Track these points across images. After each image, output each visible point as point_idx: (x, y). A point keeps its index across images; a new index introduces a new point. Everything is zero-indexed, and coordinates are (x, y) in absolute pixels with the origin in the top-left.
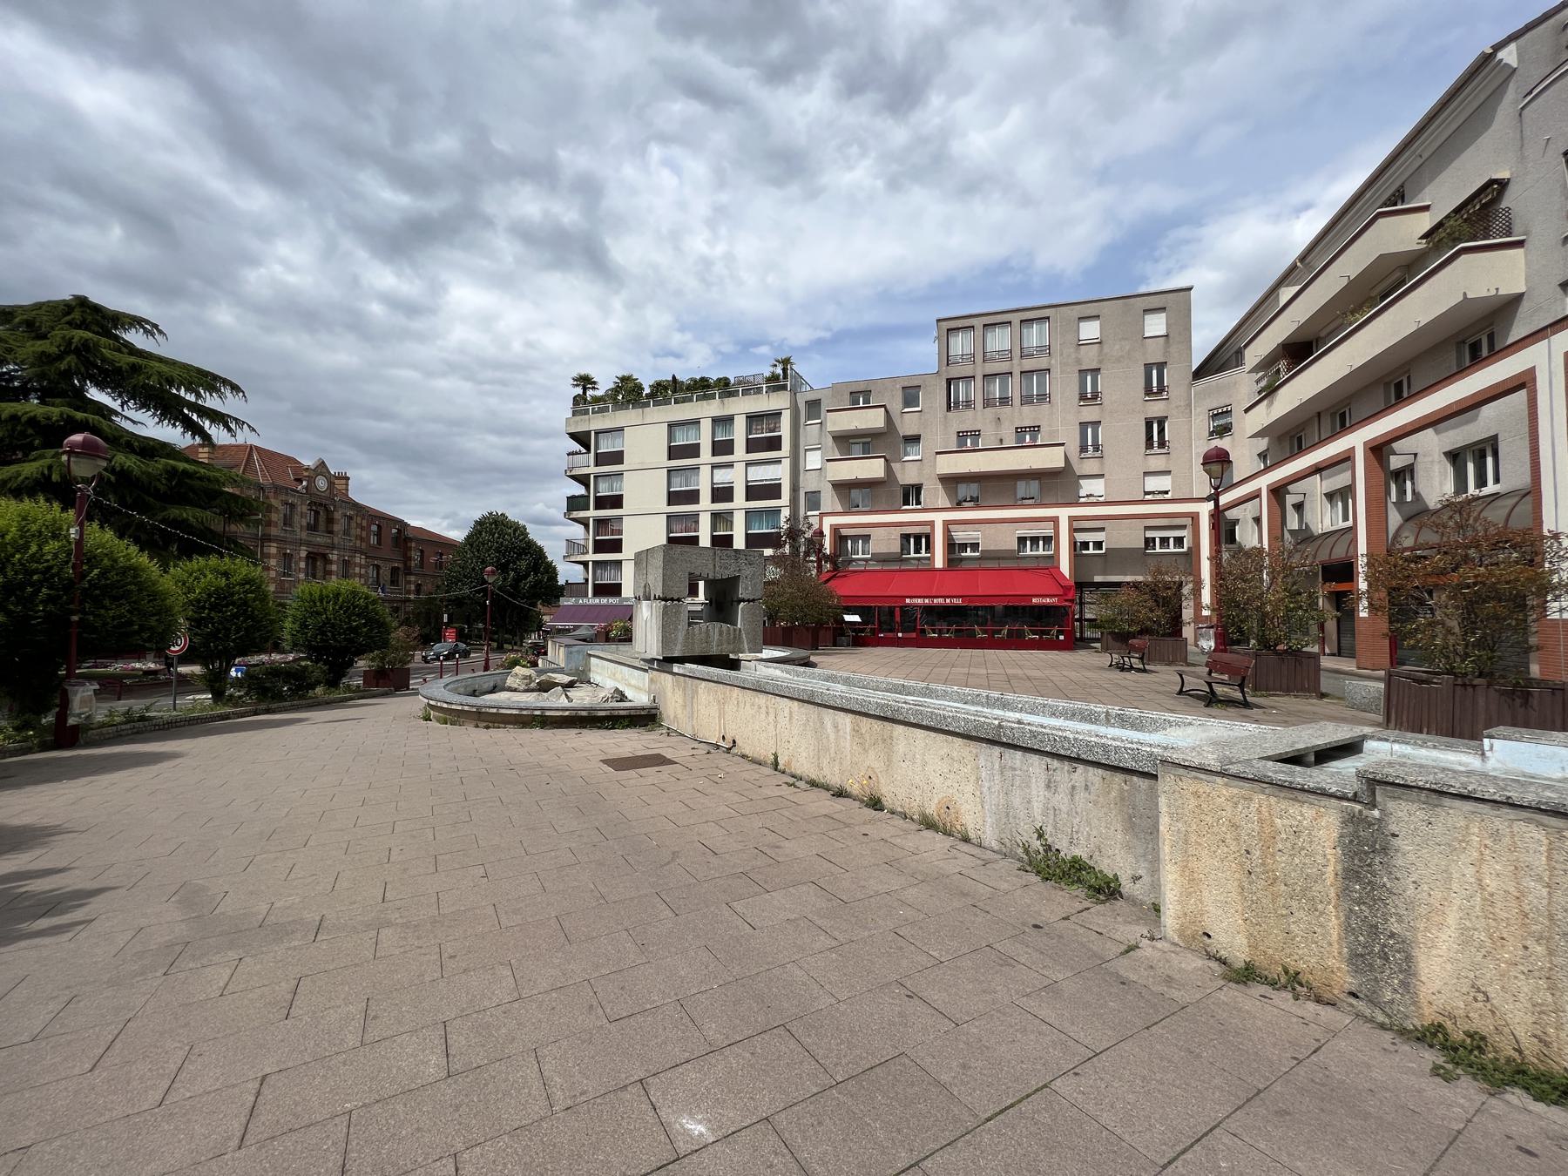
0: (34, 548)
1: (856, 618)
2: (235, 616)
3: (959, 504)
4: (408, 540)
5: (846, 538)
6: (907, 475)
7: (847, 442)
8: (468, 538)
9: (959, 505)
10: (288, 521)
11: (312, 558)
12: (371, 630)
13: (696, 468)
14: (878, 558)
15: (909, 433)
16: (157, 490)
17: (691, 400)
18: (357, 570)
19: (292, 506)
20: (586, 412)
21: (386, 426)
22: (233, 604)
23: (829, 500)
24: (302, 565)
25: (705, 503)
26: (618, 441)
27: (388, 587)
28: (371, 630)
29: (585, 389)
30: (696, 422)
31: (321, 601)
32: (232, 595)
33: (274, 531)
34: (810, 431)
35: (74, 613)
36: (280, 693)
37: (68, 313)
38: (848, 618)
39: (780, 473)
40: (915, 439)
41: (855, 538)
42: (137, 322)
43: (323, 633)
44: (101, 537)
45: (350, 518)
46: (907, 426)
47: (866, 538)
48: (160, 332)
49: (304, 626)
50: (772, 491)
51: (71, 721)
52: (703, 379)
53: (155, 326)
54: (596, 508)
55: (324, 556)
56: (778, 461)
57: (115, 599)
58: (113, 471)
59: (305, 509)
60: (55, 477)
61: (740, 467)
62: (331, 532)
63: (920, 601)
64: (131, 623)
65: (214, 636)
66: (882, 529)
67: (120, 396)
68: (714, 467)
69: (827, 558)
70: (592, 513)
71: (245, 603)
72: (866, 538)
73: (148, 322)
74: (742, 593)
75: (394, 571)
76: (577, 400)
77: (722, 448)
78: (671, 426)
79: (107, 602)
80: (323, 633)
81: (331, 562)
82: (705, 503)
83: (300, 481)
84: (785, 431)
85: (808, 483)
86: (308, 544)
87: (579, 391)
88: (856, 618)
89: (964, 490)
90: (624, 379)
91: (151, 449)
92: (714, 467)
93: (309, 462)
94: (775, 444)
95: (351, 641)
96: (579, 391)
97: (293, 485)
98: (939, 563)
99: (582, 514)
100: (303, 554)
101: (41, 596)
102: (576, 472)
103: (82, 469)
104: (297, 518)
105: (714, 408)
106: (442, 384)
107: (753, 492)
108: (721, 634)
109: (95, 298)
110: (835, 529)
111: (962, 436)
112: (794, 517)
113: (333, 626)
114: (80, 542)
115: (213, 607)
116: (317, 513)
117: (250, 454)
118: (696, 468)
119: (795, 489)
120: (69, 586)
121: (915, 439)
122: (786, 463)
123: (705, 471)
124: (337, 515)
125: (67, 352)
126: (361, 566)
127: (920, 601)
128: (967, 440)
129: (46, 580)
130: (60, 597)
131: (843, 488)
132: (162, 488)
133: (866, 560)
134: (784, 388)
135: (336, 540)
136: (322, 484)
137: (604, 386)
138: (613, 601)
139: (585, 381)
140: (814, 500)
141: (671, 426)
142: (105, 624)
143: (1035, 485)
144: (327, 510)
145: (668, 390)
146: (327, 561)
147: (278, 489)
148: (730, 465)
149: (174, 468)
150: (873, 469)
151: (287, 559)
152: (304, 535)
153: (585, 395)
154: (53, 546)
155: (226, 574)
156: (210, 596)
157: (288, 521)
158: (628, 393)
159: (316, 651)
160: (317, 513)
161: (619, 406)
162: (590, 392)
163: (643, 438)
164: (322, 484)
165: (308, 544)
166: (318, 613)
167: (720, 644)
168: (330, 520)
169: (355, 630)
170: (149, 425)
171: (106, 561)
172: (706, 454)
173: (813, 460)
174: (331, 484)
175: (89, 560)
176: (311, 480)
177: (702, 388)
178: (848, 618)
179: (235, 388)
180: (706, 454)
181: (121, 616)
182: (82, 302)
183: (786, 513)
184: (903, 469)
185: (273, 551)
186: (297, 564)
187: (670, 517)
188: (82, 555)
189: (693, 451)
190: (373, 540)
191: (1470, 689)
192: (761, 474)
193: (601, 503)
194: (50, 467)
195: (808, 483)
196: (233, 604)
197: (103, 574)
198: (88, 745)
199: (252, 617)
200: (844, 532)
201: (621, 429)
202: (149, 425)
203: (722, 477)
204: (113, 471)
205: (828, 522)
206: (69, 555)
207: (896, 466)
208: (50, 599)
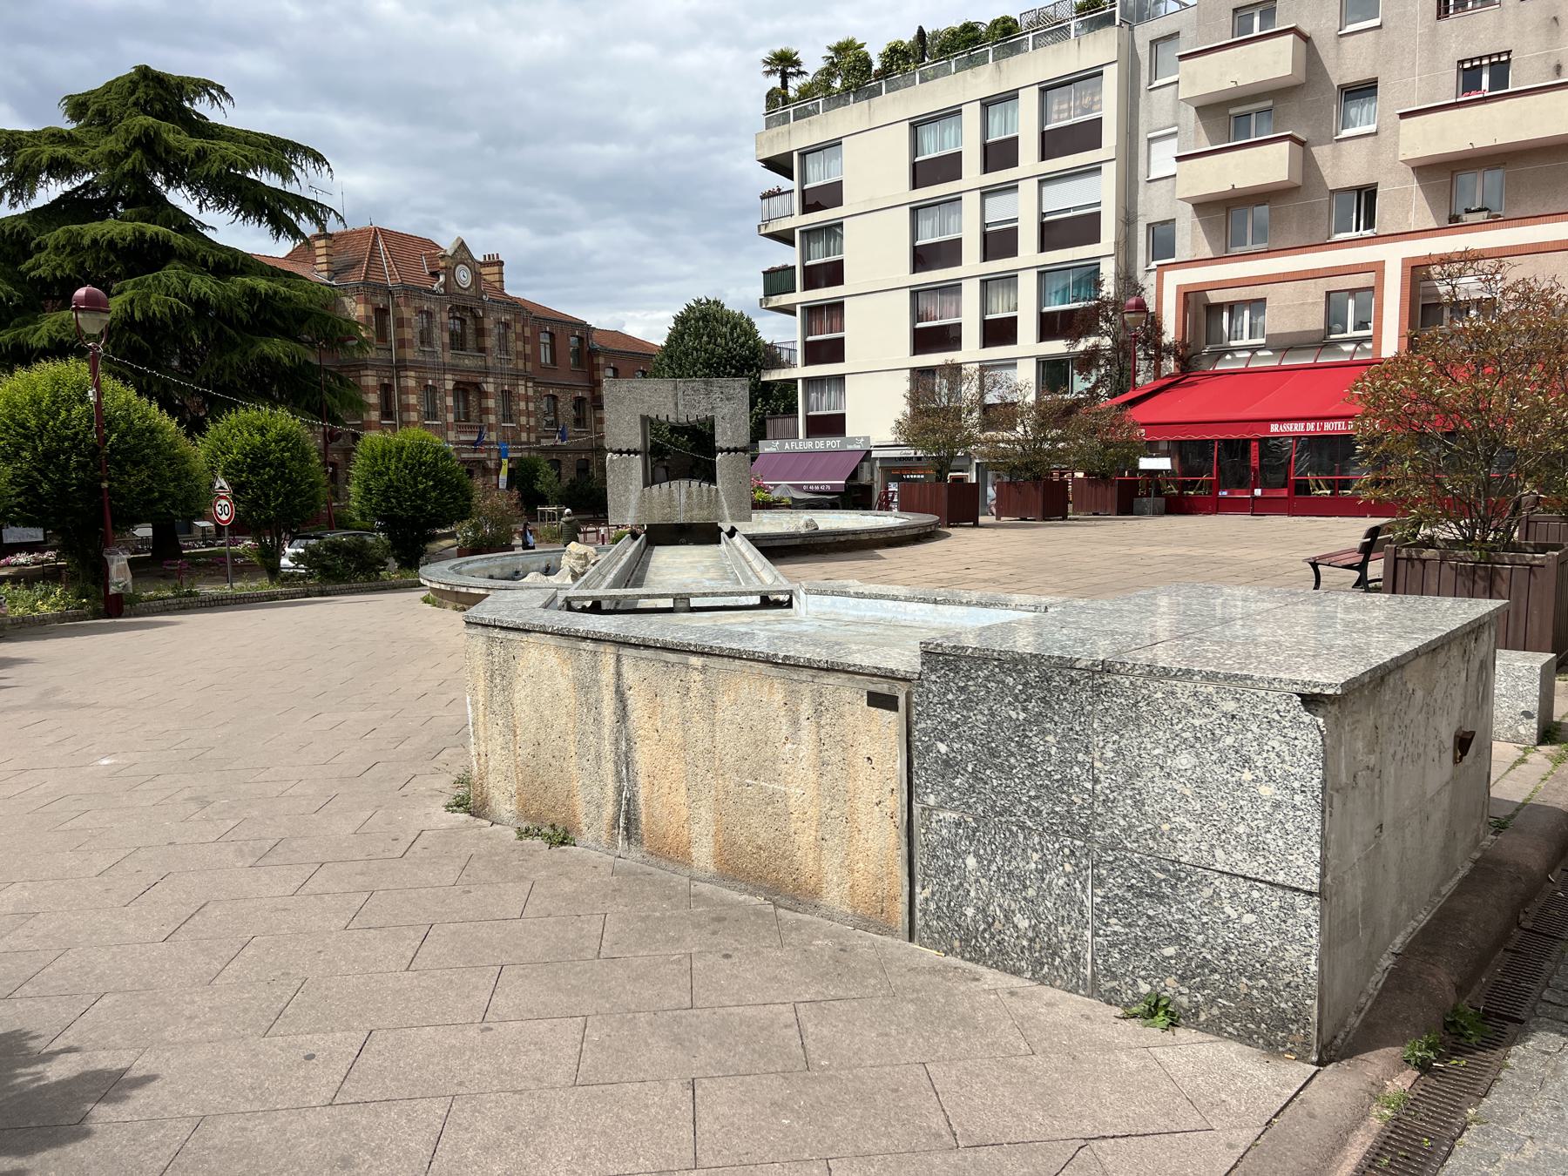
0: (64, 413)
1: (1164, 464)
2: (273, 479)
3: (1454, 219)
4: (593, 353)
5: (1219, 307)
6: (1344, 166)
7: (1229, 117)
8: (669, 340)
9: (1454, 222)
10: (425, 338)
11: (462, 389)
12: (442, 495)
13: (955, 200)
14: (1285, 345)
15: (1350, 79)
16: (240, 320)
17: (947, 72)
18: (522, 405)
19: (429, 314)
20: (786, 120)
21: (613, 152)
22: (271, 465)
23: (1190, 238)
24: (450, 401)
25: (972, 262)
26: (834, 164)
27: (572, 430)
28: (442, 495)
29: (785, 77)
30: (955, 112)
31: (383, 457)
32: (269, 453)
33: (410, 354)
34: (1158, 109)
35: (102, 480)
36: (344, 571)
37: (132, 93)
38: (1146, 464)
39: (1101, 193)
40: (1365, 90)
41: (1233, 307)
42: (203, 87)
43: (387, 500)
44: (121, 395)
45: (507, 325)
46: (1346, 66)
47: (1258, 305)
48: (227, 96)
49: (368, 490)
50: (1084, 228)
51: (113, 590)
52: (969, 28)
53: (221, 89)
54: (806, 287)
55: (477, 386)
56: (1094, 169)
57: (136, 464)
58: (189, 301)
59: (445, 316)
60: (138, 315)
61: (1028, 189)
62: (482, 350)
63: (1298, 427)
64: (150, 490)
65: (254, 503)
66: (1284, 286)
67: (197, 193)
68: (986, 193)
69: (1169, 350)
70: (800, 297)
71: (283, 464)
72: (1258, 305)
73: (213, 85)
74: (720, 442)
75: (579, 402)
76: (775, 99)
77: (999, 154)
78: (915, 125)
79: (128, 468)
80: (387, 500)
81: (485, 395)
82: (972, 262)
83: (435, 275)
84: (1108, 109)
85: (1153, 207)
86: (454, 369)
87: (776, 81)
88: (1164, 464)
89: (1479, 187)
90: (842, 49)
91: (233, 264)
92: (986, 193)
93: (447, 244)
94: (1088, 136)
95: (419, 509)
96: (776, 81)
97: (426, 282)
98: (1390, 345)
99: (785, 300)
100: (450, 385)
101: (73, 464)
102: (770, 229)
103: (92, 324)
104: (436, 332)
105: (982, 80)
106: (691, 60)
107: (1053, 233)
108: (689, 495)
109: (156, 67)
110: (1191, 298)
111: (1469, 75)
112: (1127, 279)
113: (398, 490)
114: (98, 404)
115: (252, 469)
116: (463, 321)
117: (375, 243)
118: (955, 200)
119: (1128, 219)
120: (95, 451)
121: (1365, 90)
122: (1110, 172)
123: (971, 202)
124: (489, 323)
125: (131, 148)
126: (527, 399)
127: (1298, 427)
128: (1484, 77)
129: (75, 446)
130: (88, 464)
131: (1222, 211)
132: (244, 317)
133: (1253, 349)
134: (1109, 20)
135: (490, 362)
136: (464, 276)
137: (813, 62)
138: (832, 443)
139: (784, 63)
140: (1163, 241)
141: (915, 125)
142: (131, 491)
143: (1494, 178)
144: (476, 317)
145: (916, 55)
146: (484, 395)
147: (410, 291)
148: (1011, 187)
149: (253, 289)
150: (1266, 165)
151: (430, 392)
152: (448, 357)
153: (791, 89)
154: (78, 410)
155: (262, 430)
156: (246, 456)
157: (425, 338)
158: (854, 75)
159: (391, 523)
160: (463, 321)
161: (837, 100)
162: (794, 83)
163: (870, 153)
164: (464, 276)
165: (454, 369)
166: (381, 474)
167: (690, 508)
168: (480, 332)
169: (423, 495)
170: (232, 230)
171: (123, 425)
172: (972, 173)
173: (1162, 159)
174: (477, 277)
175: (109, 423)
176: (450, 272)
177: (964, 44)
178: (1146, 464)
179: (318, 158)
180: (972, 173)
181: (143, 482)
182: (144, 73)
183: (1108, 270)
184: (1337, 157)
185: (412, 383)
186: (443, 400)
187: (915, 294)
188: (101, 418)
189: (949, 167)
190: (545, 356)
191: (1418, 565)
192: (1066, 199)
193: (814, 277)
194: (132, 301)
195: (1153, 207)
196: (271, 465)
197: (122, 437)
198: (137, 615)
199: (291, 481)
200: (1215, 297)
201: (836, 143)
202: (232, 230)
203: (999, 210)
204: (189, 301)
205: (1175, 280)
206: (90, 420)
207: (1321, 153)
208: (82, 466)
